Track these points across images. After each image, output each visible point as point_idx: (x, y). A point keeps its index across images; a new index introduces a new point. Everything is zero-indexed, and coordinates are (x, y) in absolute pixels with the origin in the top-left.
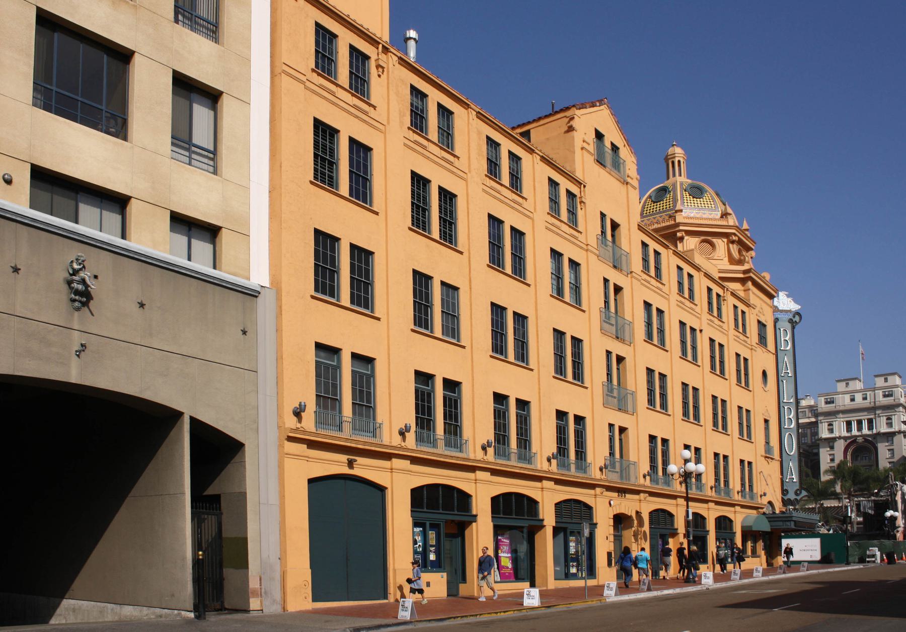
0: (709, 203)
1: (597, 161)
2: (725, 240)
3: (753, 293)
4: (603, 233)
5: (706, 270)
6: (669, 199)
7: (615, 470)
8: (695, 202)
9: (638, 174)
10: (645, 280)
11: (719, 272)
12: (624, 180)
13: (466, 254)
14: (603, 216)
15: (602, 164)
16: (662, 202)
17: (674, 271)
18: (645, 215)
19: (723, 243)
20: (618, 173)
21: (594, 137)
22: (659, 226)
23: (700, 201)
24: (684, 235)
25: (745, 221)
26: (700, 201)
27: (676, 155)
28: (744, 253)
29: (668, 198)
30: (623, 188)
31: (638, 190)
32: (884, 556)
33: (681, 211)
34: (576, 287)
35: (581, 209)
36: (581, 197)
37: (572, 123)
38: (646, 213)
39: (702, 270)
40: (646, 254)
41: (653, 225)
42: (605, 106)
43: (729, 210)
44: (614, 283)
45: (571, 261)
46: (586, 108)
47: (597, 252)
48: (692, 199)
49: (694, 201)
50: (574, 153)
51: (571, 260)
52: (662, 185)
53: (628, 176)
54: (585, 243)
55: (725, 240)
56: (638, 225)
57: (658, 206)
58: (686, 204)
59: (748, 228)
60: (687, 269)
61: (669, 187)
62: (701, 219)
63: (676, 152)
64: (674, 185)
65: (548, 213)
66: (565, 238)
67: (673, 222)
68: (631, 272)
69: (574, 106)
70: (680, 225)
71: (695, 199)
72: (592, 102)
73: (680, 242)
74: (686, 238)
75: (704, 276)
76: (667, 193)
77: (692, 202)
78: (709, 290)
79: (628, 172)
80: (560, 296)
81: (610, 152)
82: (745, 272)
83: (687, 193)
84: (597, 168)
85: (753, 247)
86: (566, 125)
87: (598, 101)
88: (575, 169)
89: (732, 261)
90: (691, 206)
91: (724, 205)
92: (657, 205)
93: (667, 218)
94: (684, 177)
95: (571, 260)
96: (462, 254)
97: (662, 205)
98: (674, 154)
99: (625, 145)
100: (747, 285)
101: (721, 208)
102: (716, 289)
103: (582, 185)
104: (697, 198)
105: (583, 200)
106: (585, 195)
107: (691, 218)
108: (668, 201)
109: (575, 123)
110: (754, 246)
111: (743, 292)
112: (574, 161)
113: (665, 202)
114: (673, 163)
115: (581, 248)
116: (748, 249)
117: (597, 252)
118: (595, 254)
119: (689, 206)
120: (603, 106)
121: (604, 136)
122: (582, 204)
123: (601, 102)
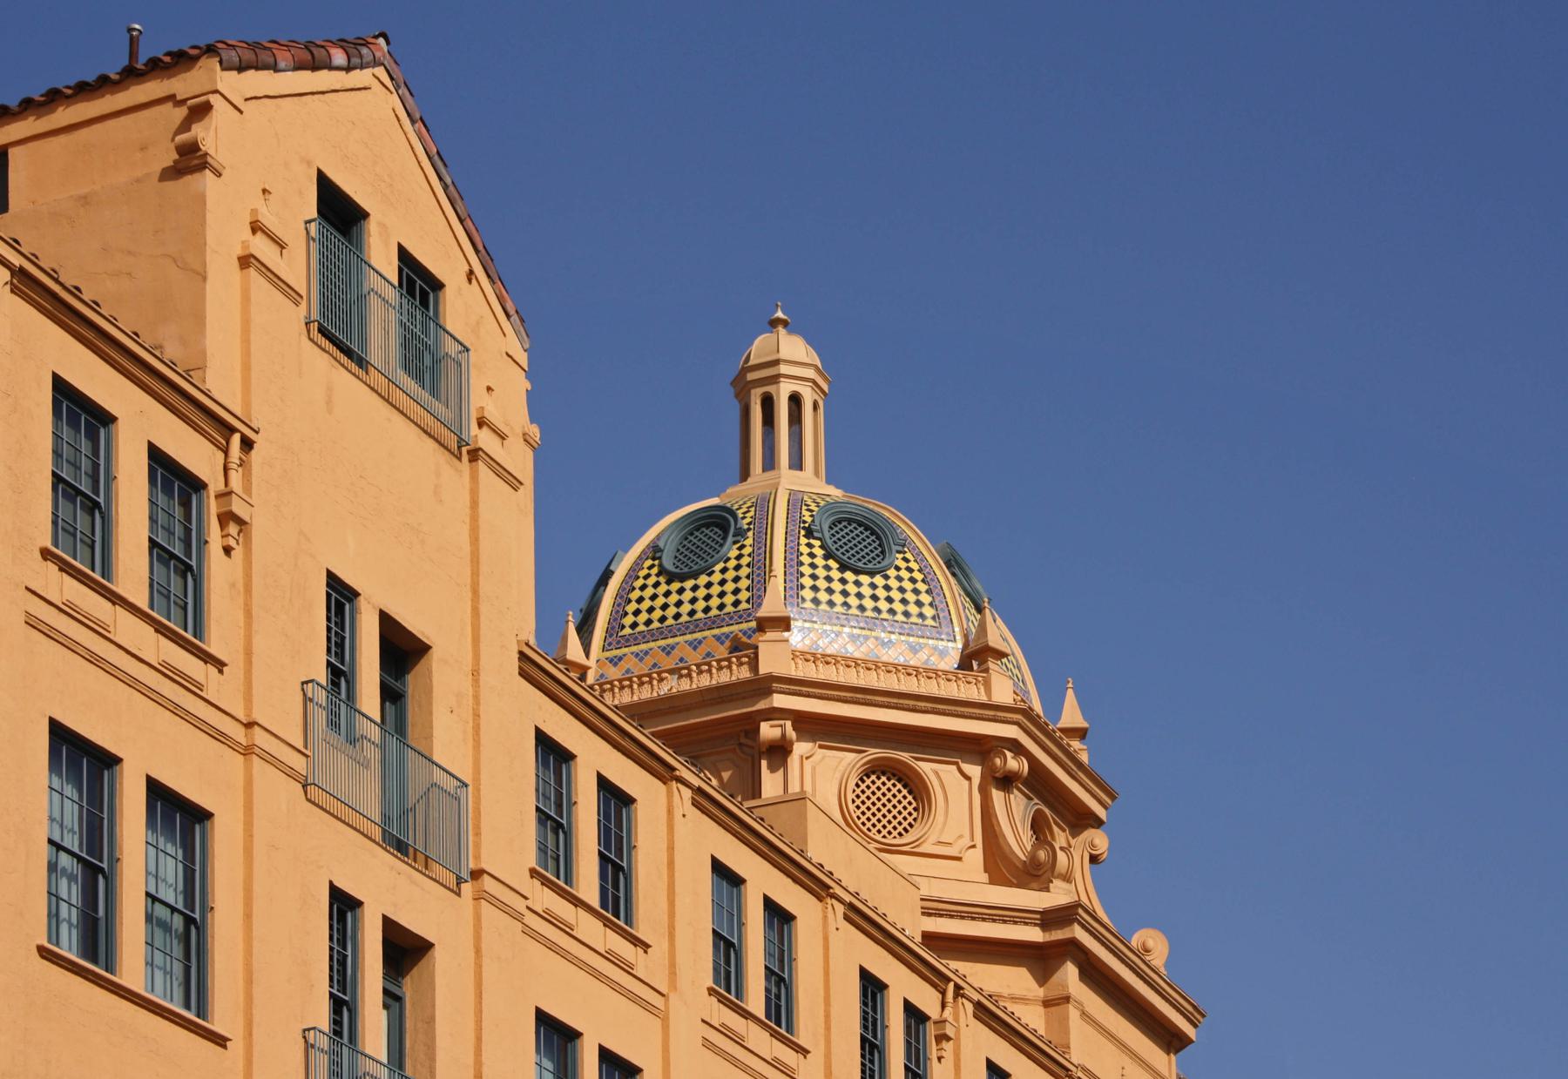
0: (911, 597)
1: (323, 331)
2: (975, 771)
3: (1084, 1015)
4: (340, 674)
5: (856, 895)
6: (737, 568)
8: (851, 588)
9: (534, 418)
10: (549, 918)
11: (927, 913)
12: (460, 439)
13: (236, 1046)
14: (341, 596)
15: (348, 352)
16: (703, 579)
17: (699, 888)
18: (627, 631)
20: (425, 396)
21: (315, 214)
22: (685, 685)
23: (873, 586)
24: (791, 733)
25: (1070, 693)
26: (873, 586)
27: (784, 369)
28: (1060, 838)
29: (732, 563)
30: (455, 476)
31: (526, 494)
34: (189, 921)
35: (228, 550)
36: (225, 495)
37: (198, 131)
38: (634, 625)
39: (838, 891)
40: (559, 795)
41: (661, 680)
42: (380, 72)
43: (998, 634)
44: (385, 918)
45: (159, 794)
46: (275, 68)
47: (298, 763)
48: (835, 574)
49: (843, 581)
50: (205, 279)
51: (157, 792)
52: (714, 501)
53: (481, 423)
54: (241, 716)
55: (975, 771)
56: (523, 656)
57: (688, 595)
58: (808, 594)
59: (1086, 725)
60: (762, 880)
61: (740, 514)
62: (874, 665)
63: (784, 353)
64: (764, 506)
65: (46, 554)
66: (133, 683)
67: (744, 673)
68: (477, 874)
69: (211, 50)
71: (849, 576)
72: (309, 46)
73: (773, 769)
74: (801, 748)
75: (846, 918)
76: (730, 539)
77: (837, 586)
78: (872, 987)
79: (478, 400)
80: (95, 961)
81: (392, 295)
82: (1050, 918)
83: (817, 543)
84: (320, 363)
85: (1101, 813)
86: (173, 140)
87: (342, 43)
88: (203, 353)
89: (1000, 866)
90: (831, 603)
91: (979, 609)
92: (681, 591)
93: (722, 651)
94: (817, 473)
95: (157, 792)
96: (225, 1047)
97: (702, 593)
98: (776, 362)
99: (471, 274)
100: (1056, 978)
101: (961, 616)
102: (903, 985)
103: (236, 438)
104: (857, 572)
105: (238, 507)
106: (248, 487)
107: (827, 659)
108: (730, 575)
109: (212, 135)
110: (1106, 808)
111: (1041, 1010)
112: (199, 318)
113: (717, 577)
114: (768, 403)
115: (219, 736)
116: (1080, 819)
117: (298, 763)
118: (290, 773)
119: (824, 607)
120: (368, 72)
121: (364, 215)
122: (233, 529)
123: (357, 53)
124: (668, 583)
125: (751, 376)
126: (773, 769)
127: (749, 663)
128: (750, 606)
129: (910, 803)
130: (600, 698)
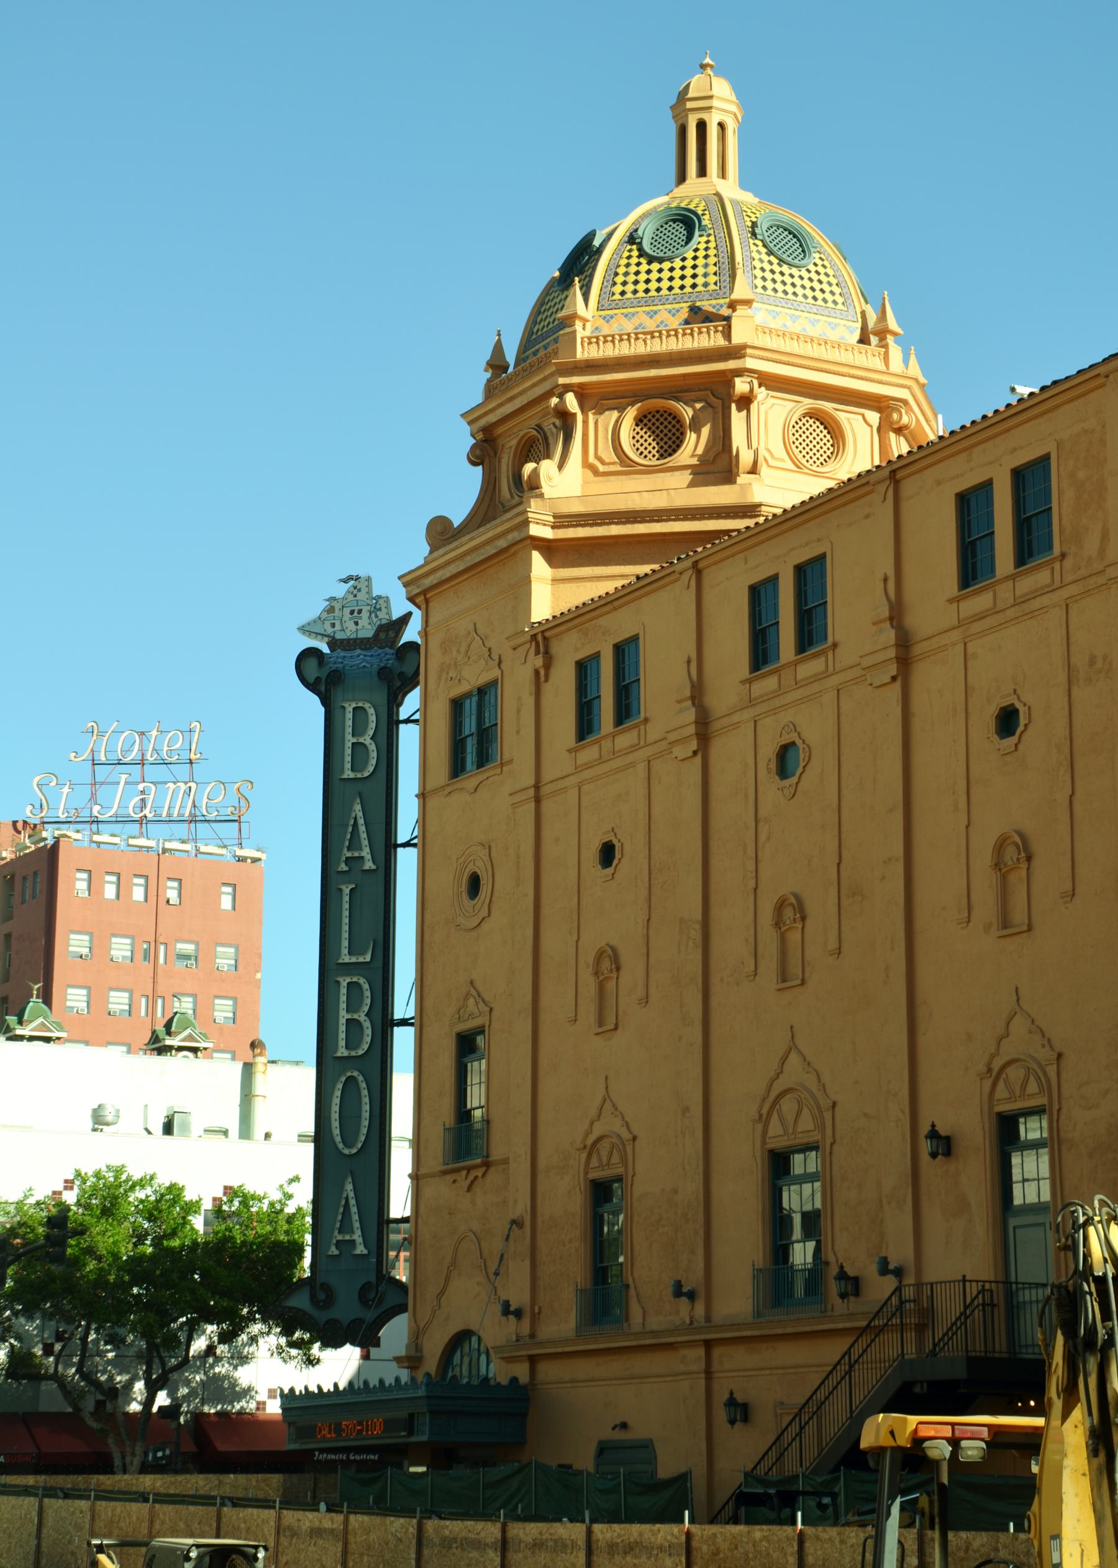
7: (1047, 1108)
19: (869, 428)
32: (412, 1469)
33: (748, 303)
67: (719, 341)
70: (749, 351)
71: (785, 269)
73: (739, 410)
77: (778, 277)
98: (711, 97)
114: (702, 126)
124: (649, 263)
125: (689, 105)
126: (739, 410)
127: (723, 332)
128: (718, 288)
129: (828, 441)
130: (828, 406)
